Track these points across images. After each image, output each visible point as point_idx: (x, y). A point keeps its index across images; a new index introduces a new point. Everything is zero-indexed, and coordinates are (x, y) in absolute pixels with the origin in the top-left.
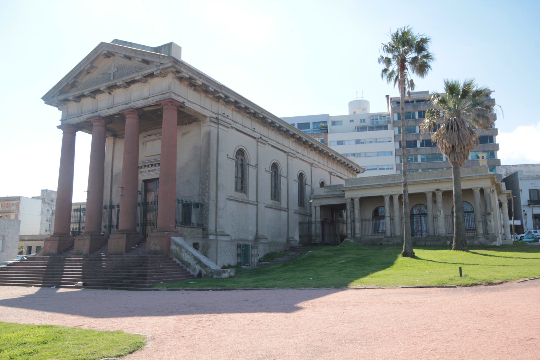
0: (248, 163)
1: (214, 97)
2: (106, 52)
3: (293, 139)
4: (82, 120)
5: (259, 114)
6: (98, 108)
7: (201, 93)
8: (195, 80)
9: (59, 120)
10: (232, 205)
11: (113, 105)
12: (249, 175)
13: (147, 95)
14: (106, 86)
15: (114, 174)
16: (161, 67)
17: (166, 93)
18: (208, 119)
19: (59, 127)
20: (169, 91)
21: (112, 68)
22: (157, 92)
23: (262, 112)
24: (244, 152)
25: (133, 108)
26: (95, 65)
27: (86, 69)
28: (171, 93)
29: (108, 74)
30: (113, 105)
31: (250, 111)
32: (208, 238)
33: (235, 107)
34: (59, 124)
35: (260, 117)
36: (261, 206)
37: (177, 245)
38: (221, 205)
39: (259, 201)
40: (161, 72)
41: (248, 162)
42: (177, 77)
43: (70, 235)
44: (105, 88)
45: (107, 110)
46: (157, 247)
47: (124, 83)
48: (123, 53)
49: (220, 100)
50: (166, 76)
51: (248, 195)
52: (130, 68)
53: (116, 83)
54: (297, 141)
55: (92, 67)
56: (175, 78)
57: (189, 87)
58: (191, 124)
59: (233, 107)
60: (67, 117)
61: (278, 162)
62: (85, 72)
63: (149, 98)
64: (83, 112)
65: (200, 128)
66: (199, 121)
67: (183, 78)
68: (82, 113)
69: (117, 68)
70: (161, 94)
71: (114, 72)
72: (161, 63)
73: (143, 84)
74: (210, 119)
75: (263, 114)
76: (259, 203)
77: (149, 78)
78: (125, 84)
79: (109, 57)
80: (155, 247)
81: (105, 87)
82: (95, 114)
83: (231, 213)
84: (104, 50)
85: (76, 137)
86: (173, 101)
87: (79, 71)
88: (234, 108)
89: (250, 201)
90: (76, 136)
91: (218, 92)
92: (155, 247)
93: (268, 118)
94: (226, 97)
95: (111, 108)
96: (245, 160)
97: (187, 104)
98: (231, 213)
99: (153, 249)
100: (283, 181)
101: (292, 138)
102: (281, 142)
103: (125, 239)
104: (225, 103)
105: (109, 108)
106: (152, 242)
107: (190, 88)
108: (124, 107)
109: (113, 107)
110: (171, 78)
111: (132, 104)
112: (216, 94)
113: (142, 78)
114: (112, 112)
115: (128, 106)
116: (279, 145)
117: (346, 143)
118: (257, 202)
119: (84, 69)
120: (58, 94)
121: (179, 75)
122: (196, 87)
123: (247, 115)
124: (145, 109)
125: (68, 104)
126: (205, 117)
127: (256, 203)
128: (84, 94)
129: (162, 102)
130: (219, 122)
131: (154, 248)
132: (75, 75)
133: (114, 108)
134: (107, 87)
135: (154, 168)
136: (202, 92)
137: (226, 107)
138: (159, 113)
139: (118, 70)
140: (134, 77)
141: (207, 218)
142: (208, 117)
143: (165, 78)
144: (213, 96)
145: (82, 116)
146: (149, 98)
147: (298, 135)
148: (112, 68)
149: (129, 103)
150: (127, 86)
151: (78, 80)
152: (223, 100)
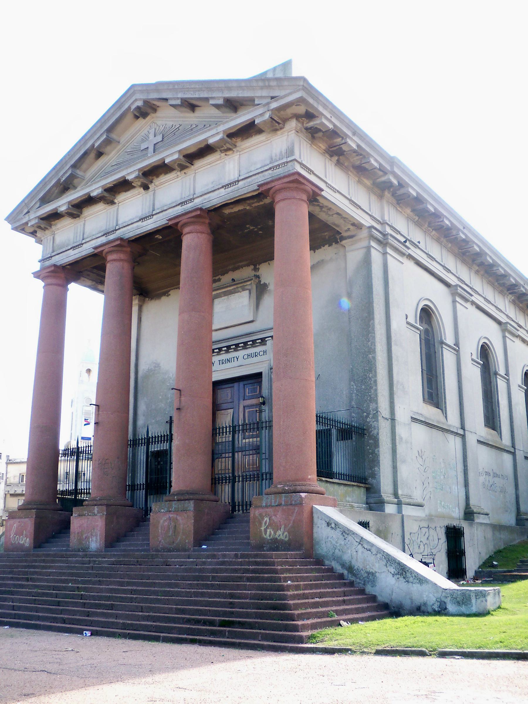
0: (441, 339)
1: (374, 184)
2: (140, 103)
3: (510, 296)
4: (84, 253)
5: (459, 230)
6: (120, 222)
7: (350, 173)
8: (343, 138)
9: (38, 261)
10: (420, 430)
11: (154, 210)
12: (445, 369)
13: (233, 176)
14: (139, 170)
15: (140, 374)
16: (274, 105)
17: (284, 163)
18: (364, 233)
19: (37, 275)
20: (289, 159)
21: (151, 136)
22: (259, 166)
23: (464, 228)
24: (431, 314)
25: (201, 209)
26: (114, 136)
27: (96, 145)
28: (296, 163)
29: (142, 151)
30: (154, 210)
31: (443, 221)
32: (383, 510)
33: (413, 211)
34: (37, 267)
35: (461, 237)
36: (471, 439)
37: (333, 525)
38: (401, 431)
39: (467, 426)
40: (271, 118)
41: (441, 337)
42: (307, 129)
43: (73, 497)
44: (139, 174)
45: (140, 223)
46: (279, 532)
47: (181, 157)
48: (180, 95)
49: (387, 194)
50: (281, 129)
51: (446, 413)
52: (192, 129)
53: (163, 159)
54: (517, 302)
55: (108, 142)
56: (302, 131)
57: (327, 155)
58: (320, 250)
59: (408, 211)
60: (53, 251)
61: (490, 342)
62: (92, 155)
63: (238, 181)
64: (85, 236)
65: (345, 256)
66: (342, 238)
67: (320, 130)
68: (83, 239)
69: (162, 134)
70: (270, 169)
71: (155, 144)
72: (272, 98)
73: (223, 155)
74: (370, 232)
75: (465, 231)
76: (466, 432)
77: (239, 140)
78: (184, 162)
79: (144, 115)
80: (275, 533)
81: (137, 173)
82: (112, 237)
83: (420, 452)
84: (136, 100)
85: (69, 293)
86: (301, 180)
87: (82, 152)
88: (411, 213)
89: (450, 426)
90: (68, 292)
91: (385, 173)
92: (275, 533)
93: (474, 242)
94: (401, 185)
95: (148, 216)
96: (433, 331)
97: (327, 193)
98: (420, 452)
99: (267, 536)
100: (501, 384)
101: (510, 293)
102: (492, 300)
103: (191, 514)
104: (394, 201)
105: (142, 219)
106: (266, 519)
107: (329, 157)
108: (179, 210)
109: (153, 215)
110: (294, 131)
111: (198, 202)
112: (381, 177)
113: (225, 137)
114: (149, 225)
115: (189, 206)
116: (490, 306)
117: (12, 485)
118: (463, 428)
119: (93, 145)
120: (38, 205)
121: (311, 124)
122: (341, 157)
123: (434, 232)
124: (227, 211)
125: (55, 225)
126: (358, 226)
127: (461, 432)
128: (91, 195)
129: (273, 184)
130: (388, 239)
131: (270, 536)
132: (72, 162)
133: (154, 217)
134: (142, 172)
135: (232, 354)
136: (351, 169)
137: (397, 209)
138: (249, 228)
139: (163, 139)
140: (206, 140)
141: (375, 461)
142: (363, 228)
143: (279, 132)
144: (371, 182)
145: (84, 246)
146: (238, 181)
147: (523, 287)
148: (151, 136)
149: (191, 200)
150: (188, 164)
151: (79, 172)
152: (391, 194)
